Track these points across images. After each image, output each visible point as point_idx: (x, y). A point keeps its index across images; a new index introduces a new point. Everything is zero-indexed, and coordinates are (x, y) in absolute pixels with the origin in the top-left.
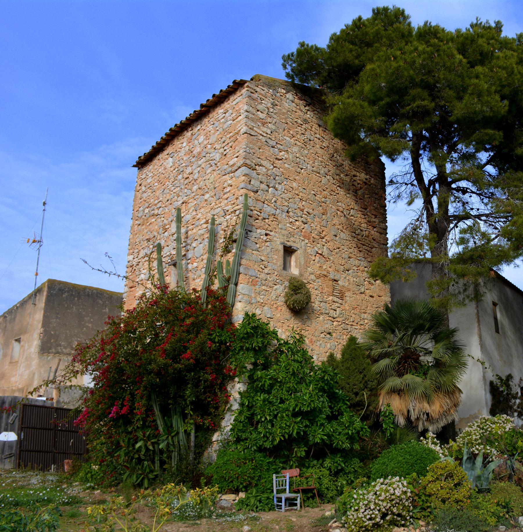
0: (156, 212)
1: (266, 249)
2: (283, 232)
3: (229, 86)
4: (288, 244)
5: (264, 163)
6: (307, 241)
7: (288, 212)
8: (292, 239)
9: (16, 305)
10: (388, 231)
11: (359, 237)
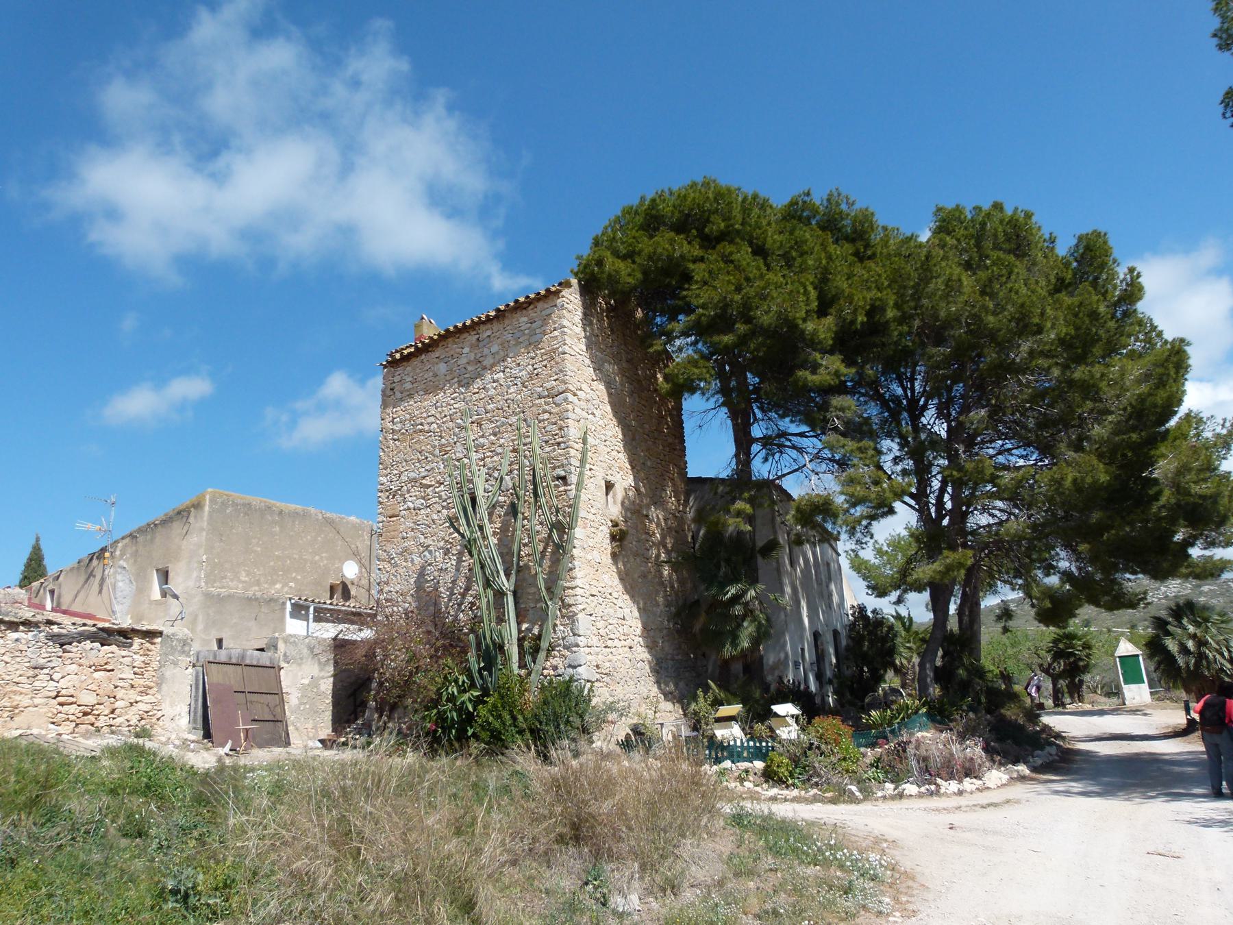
0: (426, 428)
4: (609, 478)
5: (584, 386)
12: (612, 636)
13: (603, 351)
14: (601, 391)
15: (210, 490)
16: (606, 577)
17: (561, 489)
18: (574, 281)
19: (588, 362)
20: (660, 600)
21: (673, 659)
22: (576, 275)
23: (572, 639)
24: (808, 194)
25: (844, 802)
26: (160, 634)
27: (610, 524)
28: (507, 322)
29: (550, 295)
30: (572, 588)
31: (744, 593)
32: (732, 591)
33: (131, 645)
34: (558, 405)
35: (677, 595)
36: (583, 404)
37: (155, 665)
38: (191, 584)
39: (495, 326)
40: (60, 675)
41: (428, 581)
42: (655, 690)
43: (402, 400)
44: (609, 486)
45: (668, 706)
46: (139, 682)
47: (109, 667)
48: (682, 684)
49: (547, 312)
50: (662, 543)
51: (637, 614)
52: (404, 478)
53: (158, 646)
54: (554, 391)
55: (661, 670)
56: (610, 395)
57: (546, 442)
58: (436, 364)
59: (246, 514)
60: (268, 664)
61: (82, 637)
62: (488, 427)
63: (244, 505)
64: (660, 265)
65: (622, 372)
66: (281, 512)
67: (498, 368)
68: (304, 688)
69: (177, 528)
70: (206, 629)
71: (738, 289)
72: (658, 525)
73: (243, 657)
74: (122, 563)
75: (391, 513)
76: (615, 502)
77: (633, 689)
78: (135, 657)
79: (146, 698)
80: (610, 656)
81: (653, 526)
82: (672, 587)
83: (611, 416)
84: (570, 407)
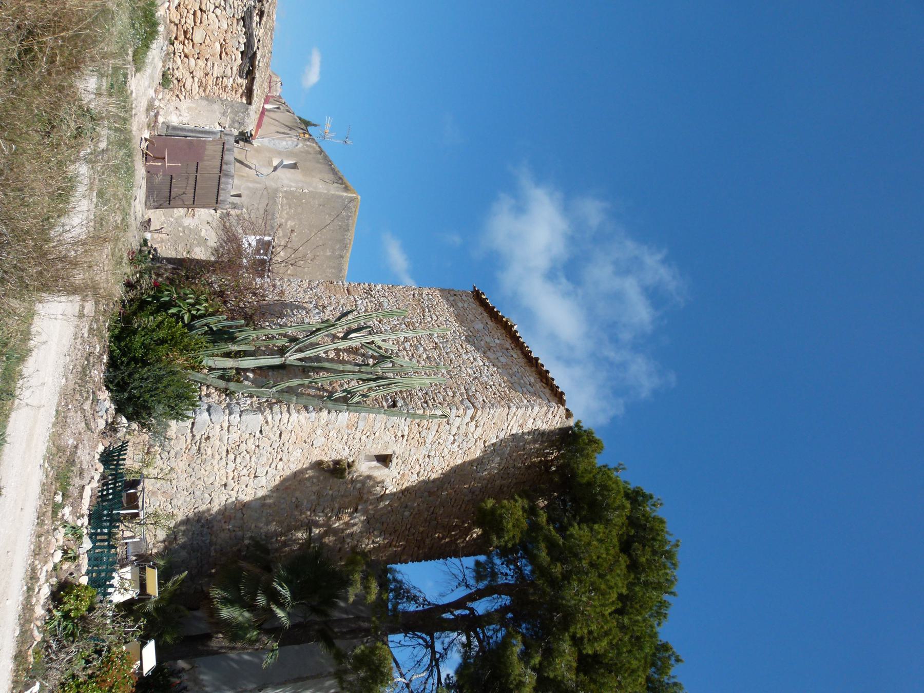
0: (427, 314)
1: (388, 436)
2: (408, 452)
3: (558, 387)
4: (394, 460)
5: (480, 430)
6: (399, 477)
7: (429, 456)
8: (400, 462)
9: (59, 405)
10: (416, 563)
11: (407, 532)
12: (238, 460)
13: (510, 455)
14: (475, 452)
15: (359, 197)
16: (297, 454)
17: (384, 403)
18: (571, 422)
19: (502, 436)
20: (273, 527)
21: (211, 544)
22: (577, 425)
23: (237, 409)
24: (678, 660)
25: (16, 671)
26: (250, 103)
27: (350, 460)
28: (527, 368)
29: (559, 397)
30: (288, 411)
31: (281, 606)
32: (286, 592)
33: (241, 77)
34: (462, 402)
35: (277, 550)
36: (462, 431)
37: (224, 96)
38: (286, 182)
39: (522, 361)
40: (219, 14)
41: (292, 311)
42: (180, 517)
43: (448, 300)
44: (384, 460)
45: (162, 534)
46: (211, 81)
47: (224, 55)
48: (184, 554)
49: (541, 394)
50: (329, 531)
51: (260, 493)
52: (382, 299)
53: (239, 100)
54: (473, 399)
55: (200, 526)
56: (471, 463)
57: (426, 394)
58: (481, 322)
59: (341, 227)
60: (220, 198)
61: (249, 36)
62: (435, 354)
63: (348, 225)
64: (600, 498)
65: (492, 479)
66: (342, 257)
67: (486, 361)
68: (197, 231)
69: (329, 177)
70: (249, 188)
71: (592, 565)
72: (347, 524)
73: (227, 175)
74: (301, 145)
75: (351, 289)
76: (370, 468)
77: (182, 484)
78: (231, 79)
79: (196, 86)
80: (217, 457)
81: (346, 518)
82: (285, 544)
83: (452, 465)
84: (461, 411)
